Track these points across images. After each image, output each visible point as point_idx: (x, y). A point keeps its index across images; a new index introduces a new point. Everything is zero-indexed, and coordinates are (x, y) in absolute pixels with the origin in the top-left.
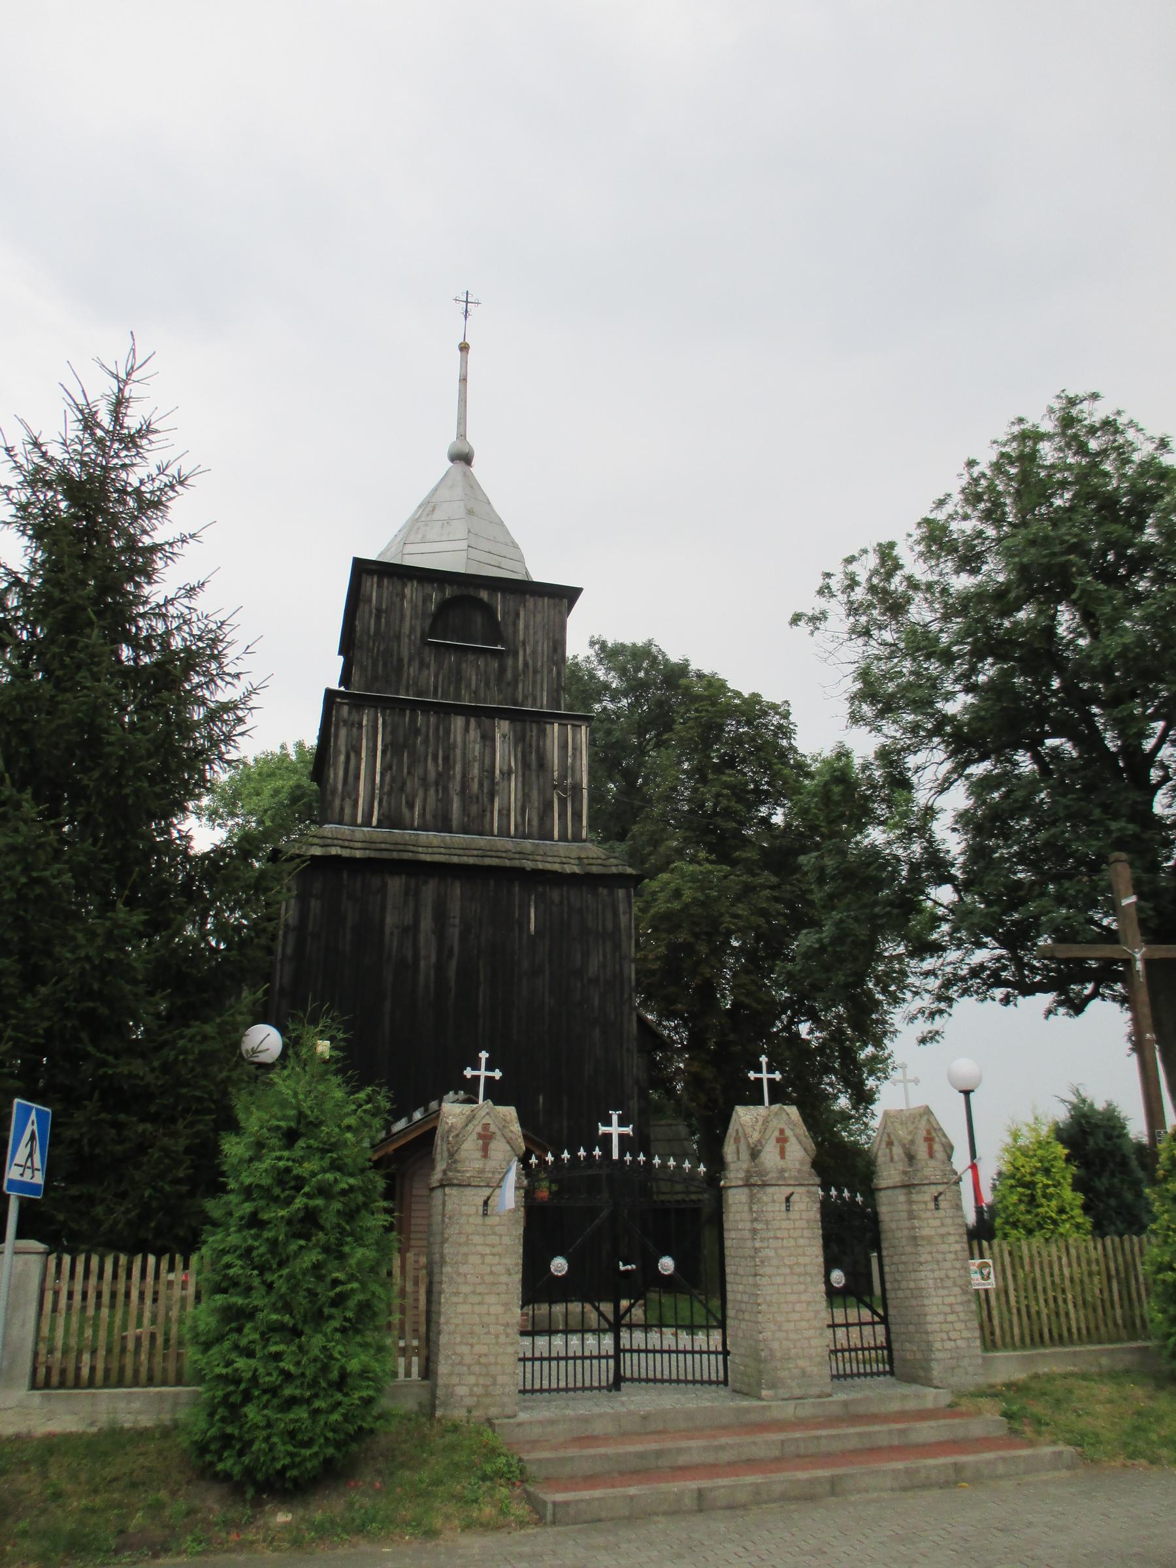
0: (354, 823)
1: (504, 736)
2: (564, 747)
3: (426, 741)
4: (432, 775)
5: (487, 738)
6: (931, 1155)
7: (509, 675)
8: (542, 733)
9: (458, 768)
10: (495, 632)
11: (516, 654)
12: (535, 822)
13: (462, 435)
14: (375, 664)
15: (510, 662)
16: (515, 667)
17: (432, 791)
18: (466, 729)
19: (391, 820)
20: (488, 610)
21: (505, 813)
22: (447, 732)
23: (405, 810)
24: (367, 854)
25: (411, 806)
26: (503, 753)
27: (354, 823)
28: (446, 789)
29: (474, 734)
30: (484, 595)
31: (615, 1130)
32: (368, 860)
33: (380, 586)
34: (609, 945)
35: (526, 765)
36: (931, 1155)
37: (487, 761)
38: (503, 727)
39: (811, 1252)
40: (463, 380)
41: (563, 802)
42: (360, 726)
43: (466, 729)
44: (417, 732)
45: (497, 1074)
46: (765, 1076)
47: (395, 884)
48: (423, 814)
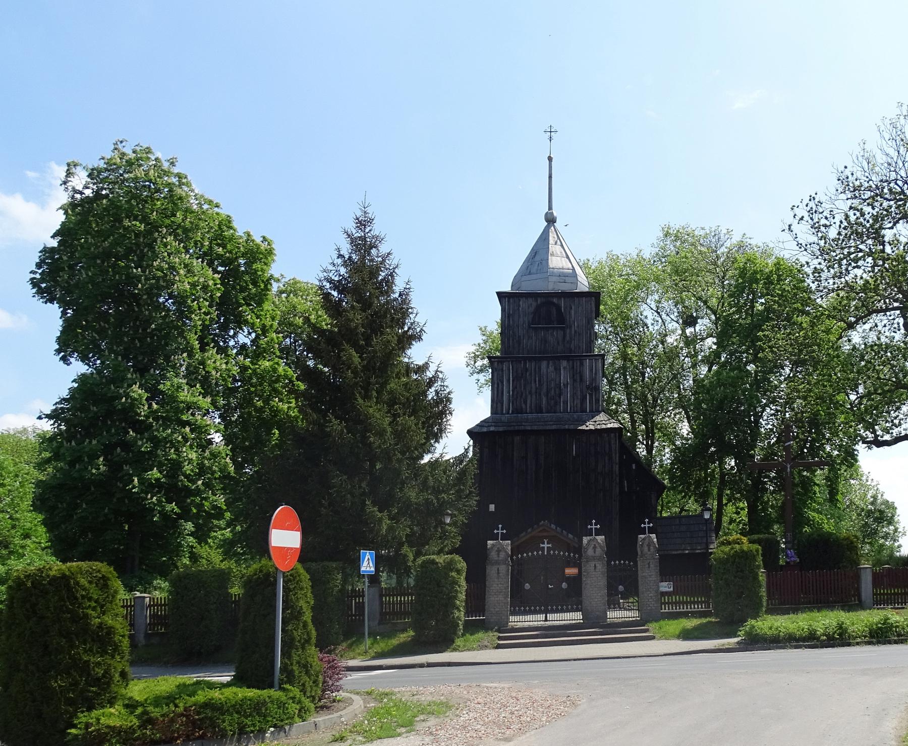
0: (502, 414)
1: (564, 368)
2: (591, 370)
3: (531, 374)
4: (534, 390)
5: (557, 370)
6: (649, 550)
7: (568, 338)
8: (582, 364)
9: (545, 384)
10: (561, 319)
11: (571, 327)
12: (579, 405)
13: (550, 208)
14: (509, 340)
15: (568, 331)
16: (570, 333)
17: (534, 396)
18: (548, 367)
19: (518, 411)
20: (558, 308)
21: (566, 403)
22: (540, 369)
23: (524, 406)
24: (505, 428)
25: (525, 403)
26: (564, 376)
27: (502, 414)
28: (540, 394)
29: (551, 368)
30: (555, 300)
31: (546, 546)
32: (504, 432)
33: (509, 302)
34: (607, 458)
35: (575, 381)
36: (649, 550)
37: (558, 379)
38: (564, 363)
39: (603, 582)
40: (550, 177)
41: (591, 395)
42: (502, 370)
43: (548, 367)
44: (527, 370)
45: (496, 531)
46: (594, 527)
47: (517, 439)
48: (531, 407)
